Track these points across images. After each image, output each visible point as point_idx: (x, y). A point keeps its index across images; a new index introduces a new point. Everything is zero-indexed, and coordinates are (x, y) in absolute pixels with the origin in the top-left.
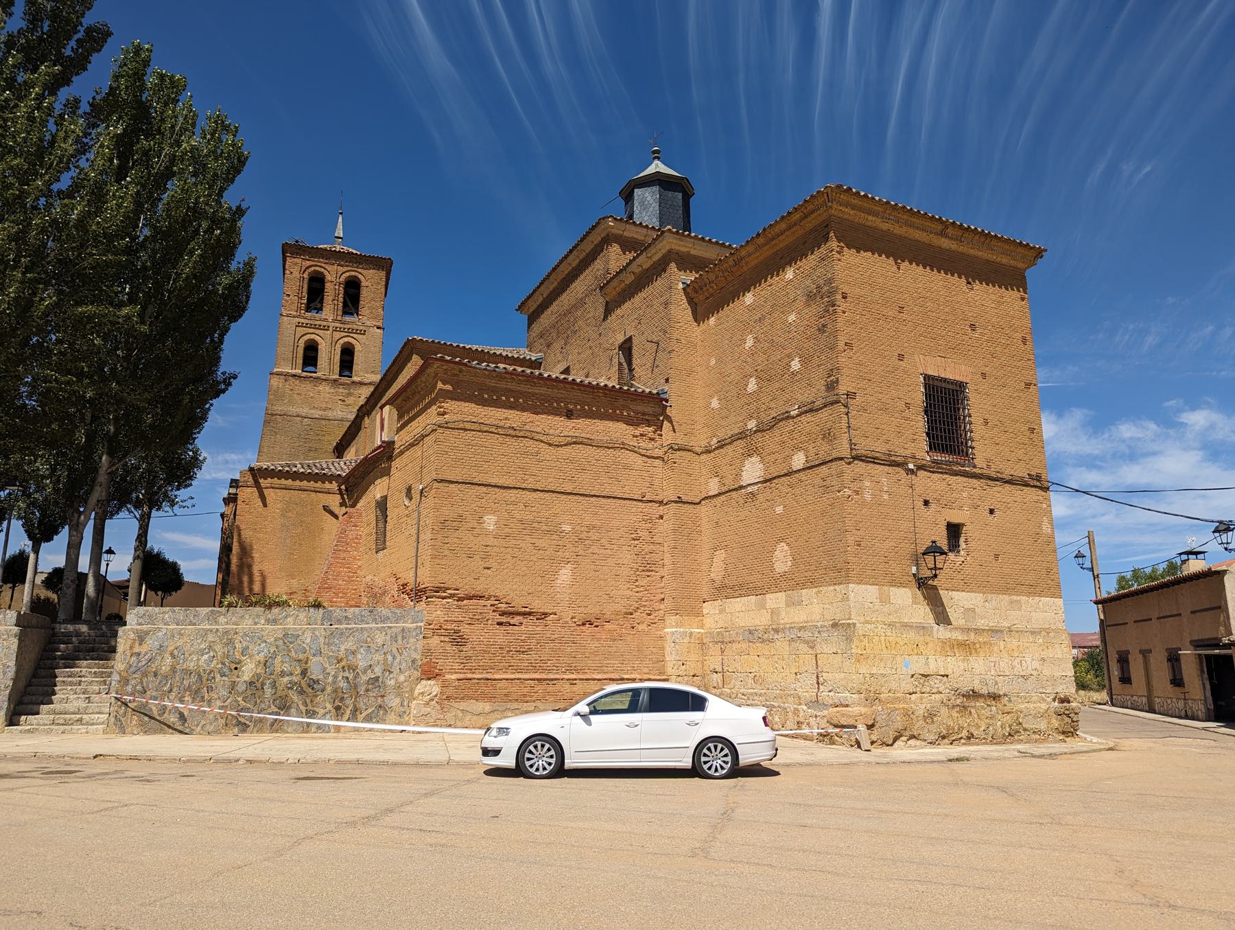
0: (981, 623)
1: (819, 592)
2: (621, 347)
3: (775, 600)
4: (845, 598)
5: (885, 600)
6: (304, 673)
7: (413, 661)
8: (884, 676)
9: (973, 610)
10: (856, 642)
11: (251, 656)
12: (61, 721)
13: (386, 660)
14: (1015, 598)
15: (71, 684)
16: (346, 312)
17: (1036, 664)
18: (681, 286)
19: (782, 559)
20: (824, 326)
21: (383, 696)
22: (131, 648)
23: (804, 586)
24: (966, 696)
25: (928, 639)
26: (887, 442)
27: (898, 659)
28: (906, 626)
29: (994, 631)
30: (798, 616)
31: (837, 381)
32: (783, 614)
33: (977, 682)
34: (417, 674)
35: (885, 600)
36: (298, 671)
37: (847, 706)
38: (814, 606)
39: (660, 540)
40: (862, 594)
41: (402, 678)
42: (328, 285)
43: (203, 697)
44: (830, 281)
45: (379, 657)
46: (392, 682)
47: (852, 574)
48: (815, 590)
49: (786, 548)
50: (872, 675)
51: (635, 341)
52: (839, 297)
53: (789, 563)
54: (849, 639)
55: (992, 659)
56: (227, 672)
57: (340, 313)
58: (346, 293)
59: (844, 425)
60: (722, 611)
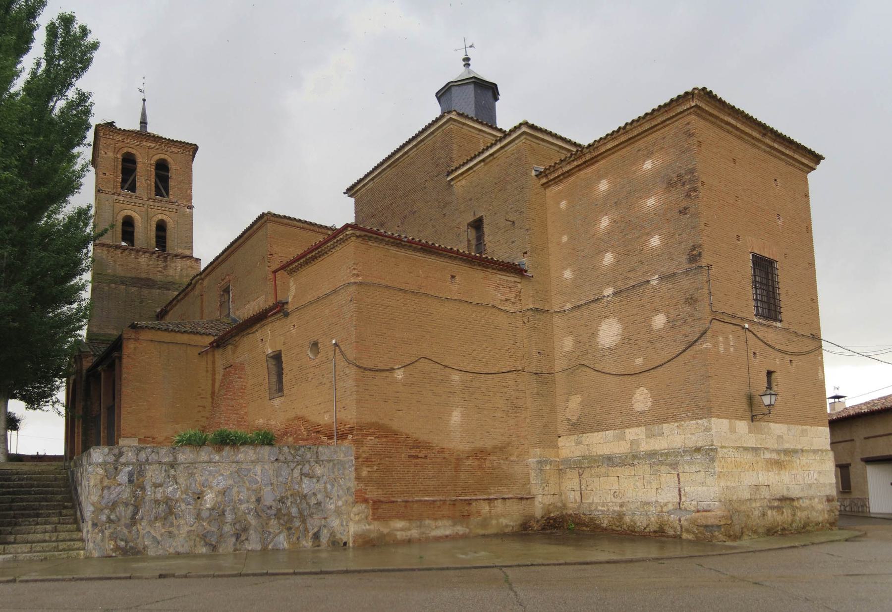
0: (787, 446)
1: (682, 425)
2: (470, 225)
3: (632, 433)
4: (708, 429)
5: (733, 430)
6: (258, 500)
7: (348, 489)
8: (734, 487)
9: (781, 437)
10: (716, 464)
11: (211, 488)
12: (38, 549)
13: (325, 488)
14: (804, 427)
15: (29, 516)
16: (158, 192)
17: (816, 476)
18: (534, 173)
19: (642, 399)
20: (685, 209)
21: (325, 518)
22: (101, 482)
23: (665, 421)
24: (780, 500)
25: (758, 459)
26: (732, 306)
27: (742, 474)
28: (746, 449)
29: (795, 451)
30: (659, 444)
31: (700, 255)
32: (643, 443)
33: (785, 490)
34: (351, 499)
35: (733, 430)
36: (253, 499)
37: (709, 511)
38: (675, 436)
39: (523, 388)
40: (719, 425)
41: (340, 503)
42: (139, 166)
43: (172, 523)
44: (692, 171)
45: (320, 486)
46: (332, 507)
47: (714, 410)
48: (676, 424)
49: (646, 391)
50: (727, 487)
51: (486, 221)
52: (700, 184)
53: (650, 404)
54: (712, 460)
55: (793, 472)
56: (192, 502)
57: (153, 193)
58: (157, 175)
59: (705, 291)
60: (579, 443)
